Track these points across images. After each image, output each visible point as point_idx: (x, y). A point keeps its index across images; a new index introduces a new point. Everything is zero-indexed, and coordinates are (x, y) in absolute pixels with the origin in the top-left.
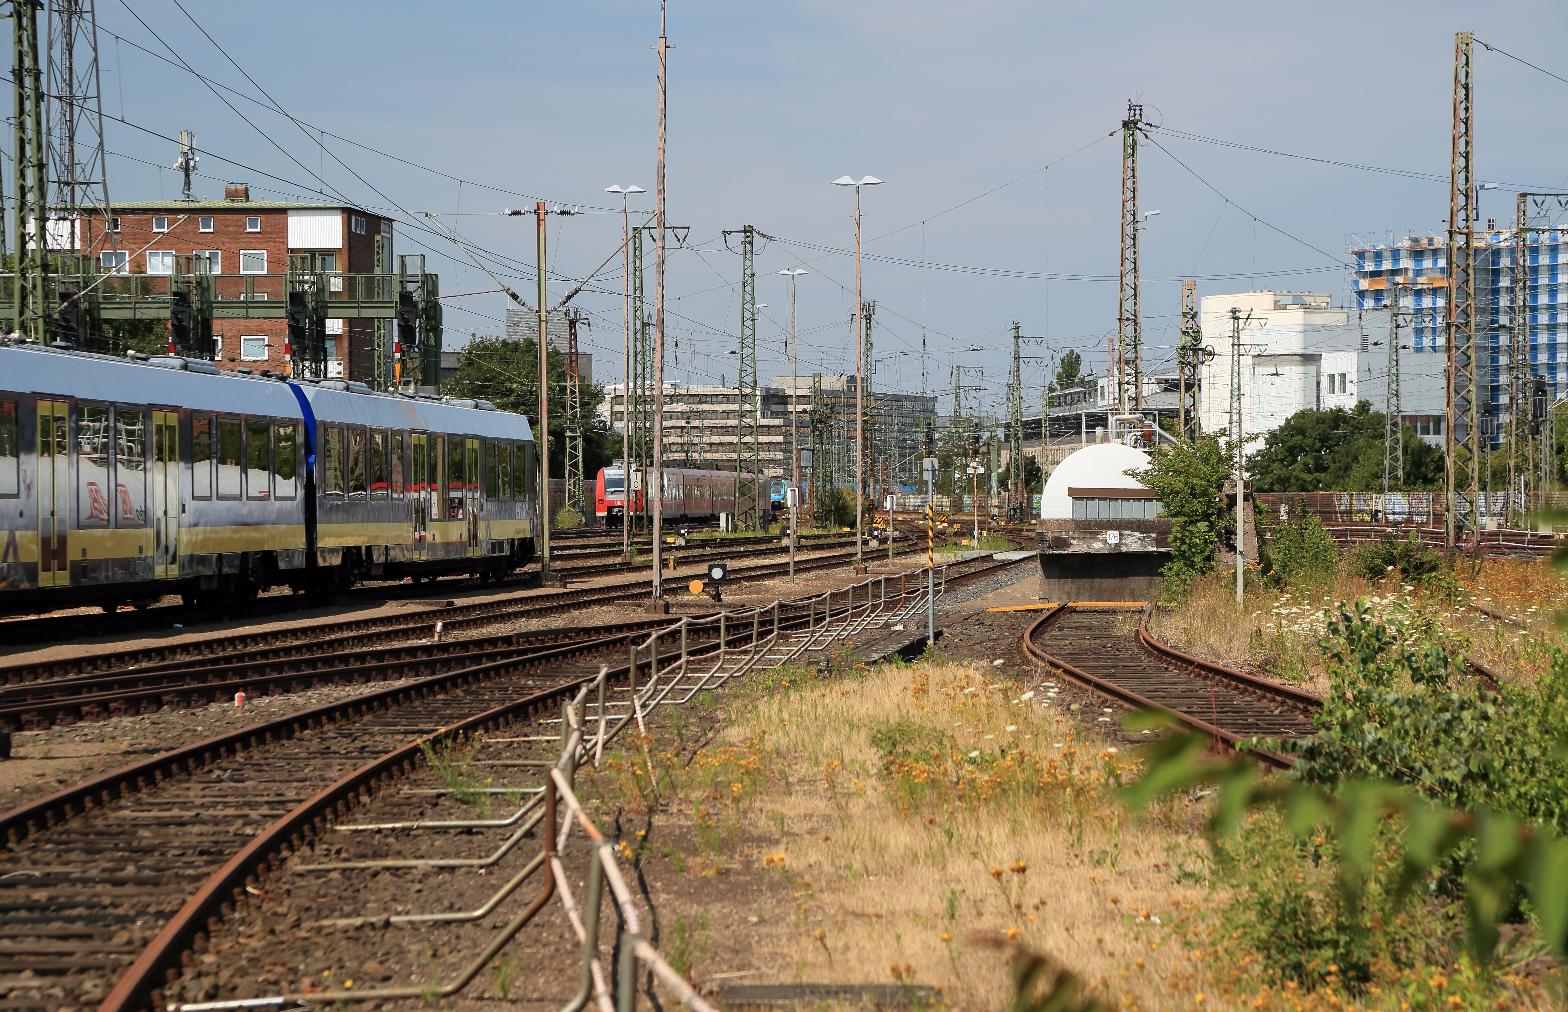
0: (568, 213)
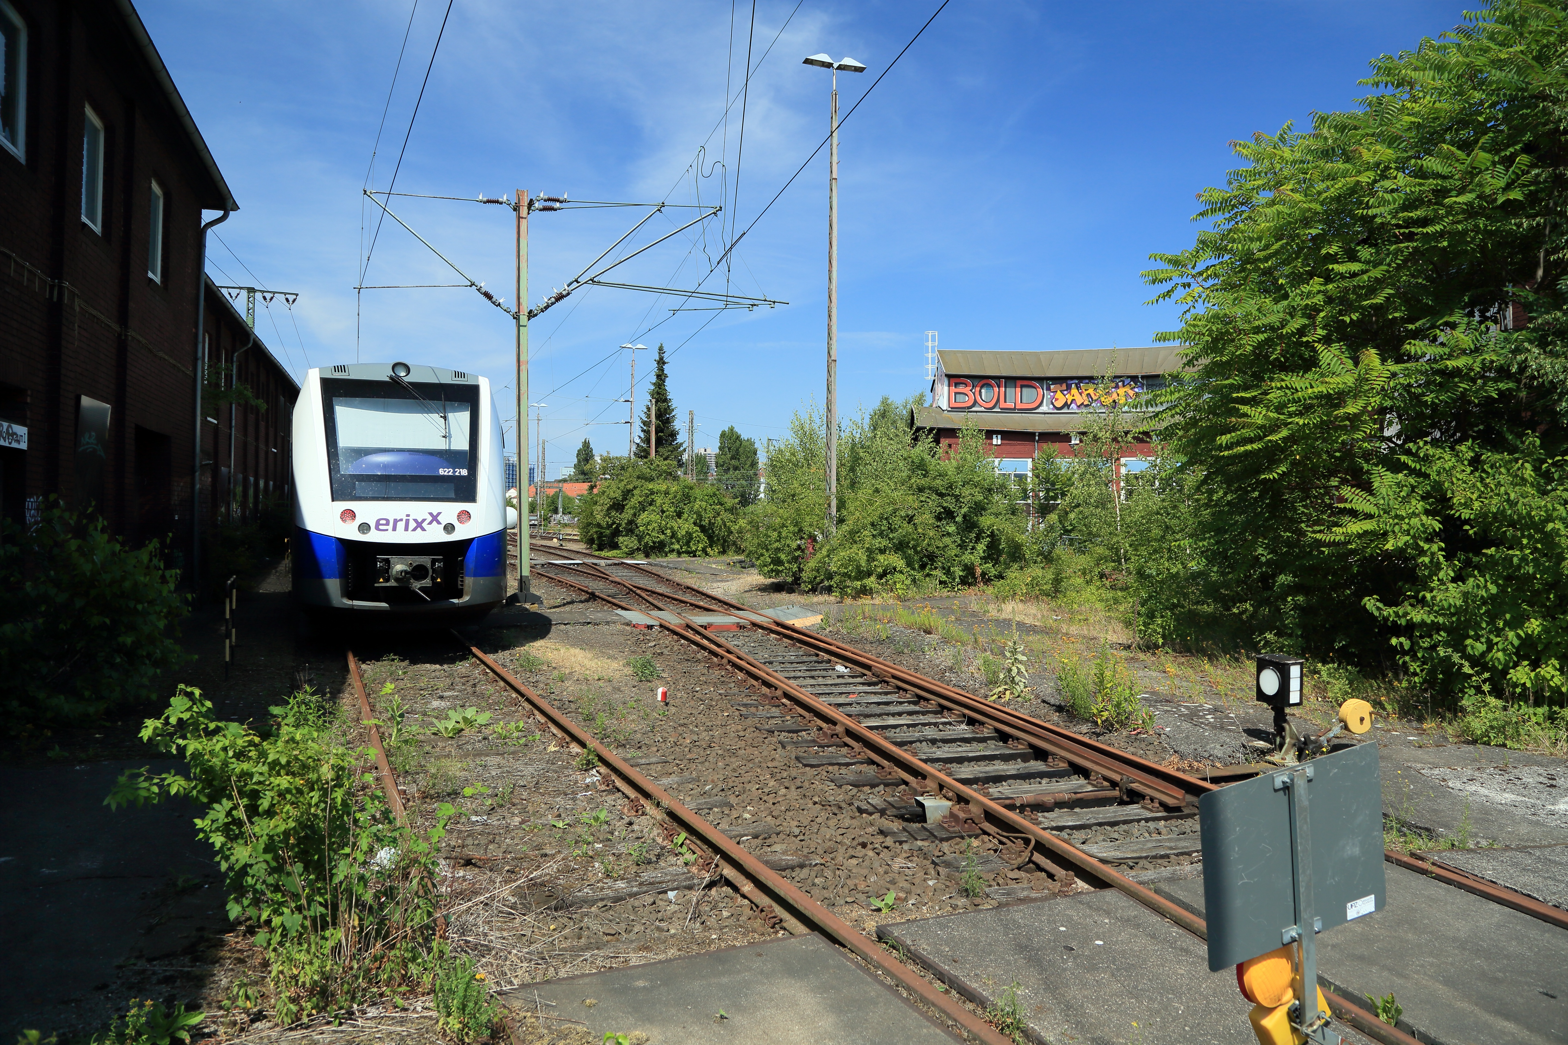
0: (497, 202)
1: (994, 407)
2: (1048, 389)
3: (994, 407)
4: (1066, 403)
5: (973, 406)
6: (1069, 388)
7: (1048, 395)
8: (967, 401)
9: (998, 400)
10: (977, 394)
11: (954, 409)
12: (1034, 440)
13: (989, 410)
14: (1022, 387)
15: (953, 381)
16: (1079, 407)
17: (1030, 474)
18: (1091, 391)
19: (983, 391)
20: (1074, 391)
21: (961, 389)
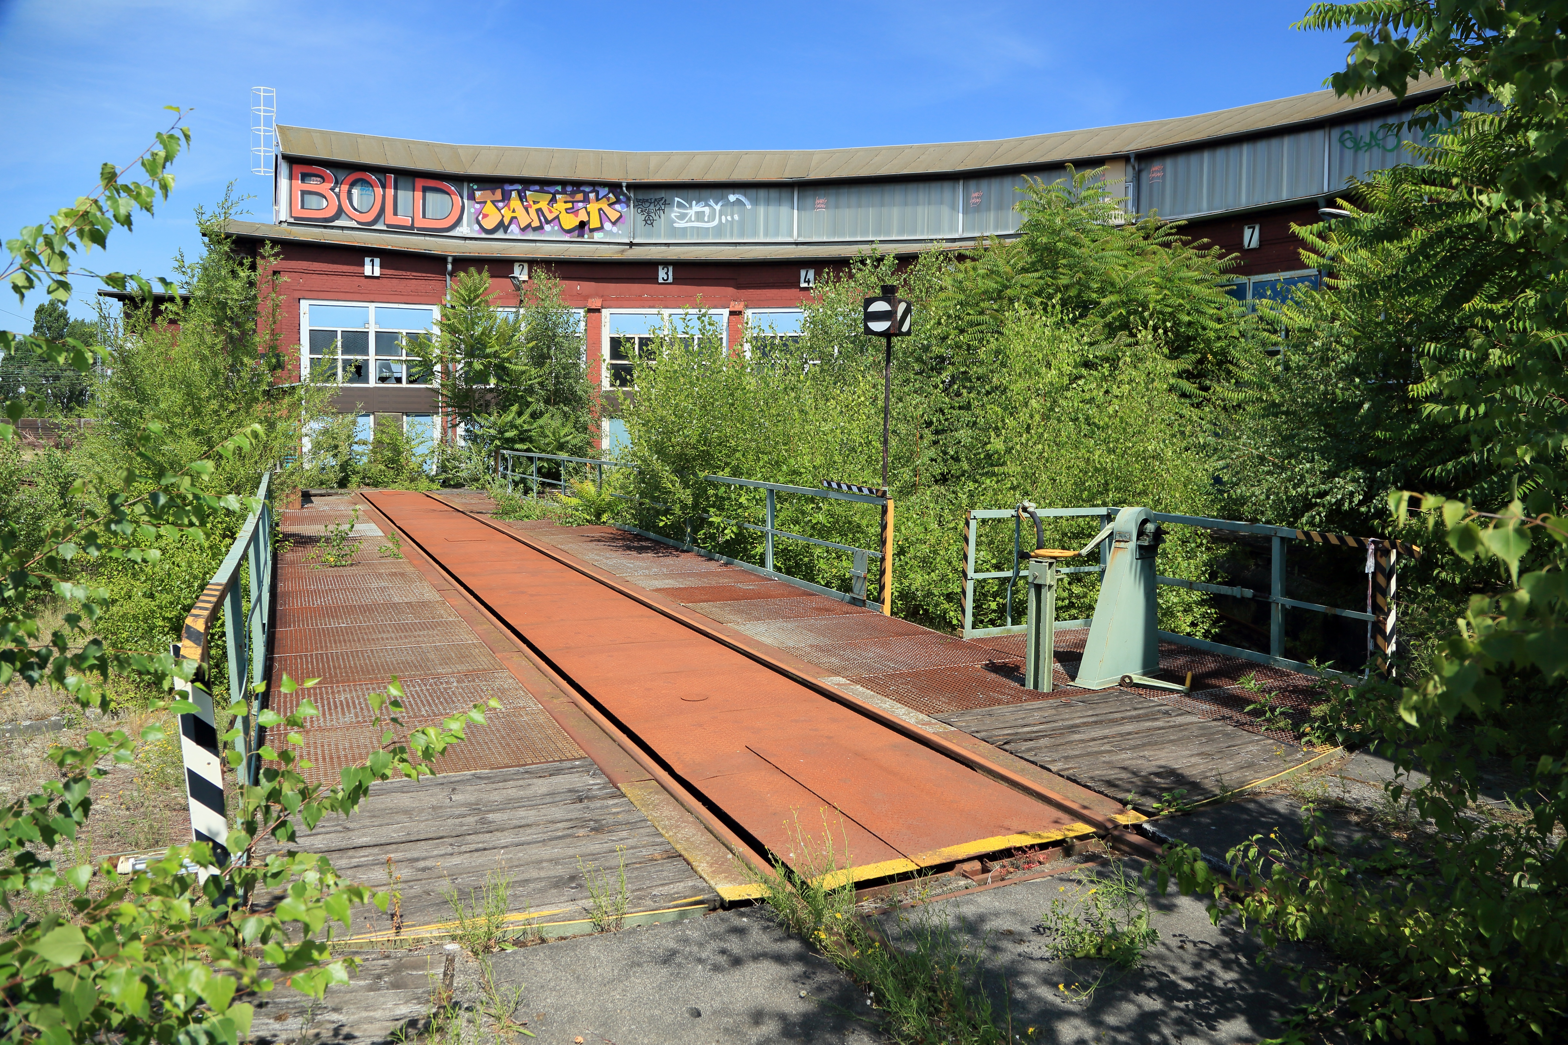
1: (375, 221)
2: (472, 197)
3: (375, 221)
4: (502, 221)
5: (337, 216)
6: (506, 197)
7: (471, 208)
8: (324, 207)
9: (382, 210)
10: (343, 196)
11: (299, 221)
12: (443, 272)
13: (366, 227)
14: (425, 190)
15: (299, 169)
16: (523, 230)
17: (436, 330)
18: (543, 205)
19: (355, 192)
20: (515, 203)
21: (313, 184)
